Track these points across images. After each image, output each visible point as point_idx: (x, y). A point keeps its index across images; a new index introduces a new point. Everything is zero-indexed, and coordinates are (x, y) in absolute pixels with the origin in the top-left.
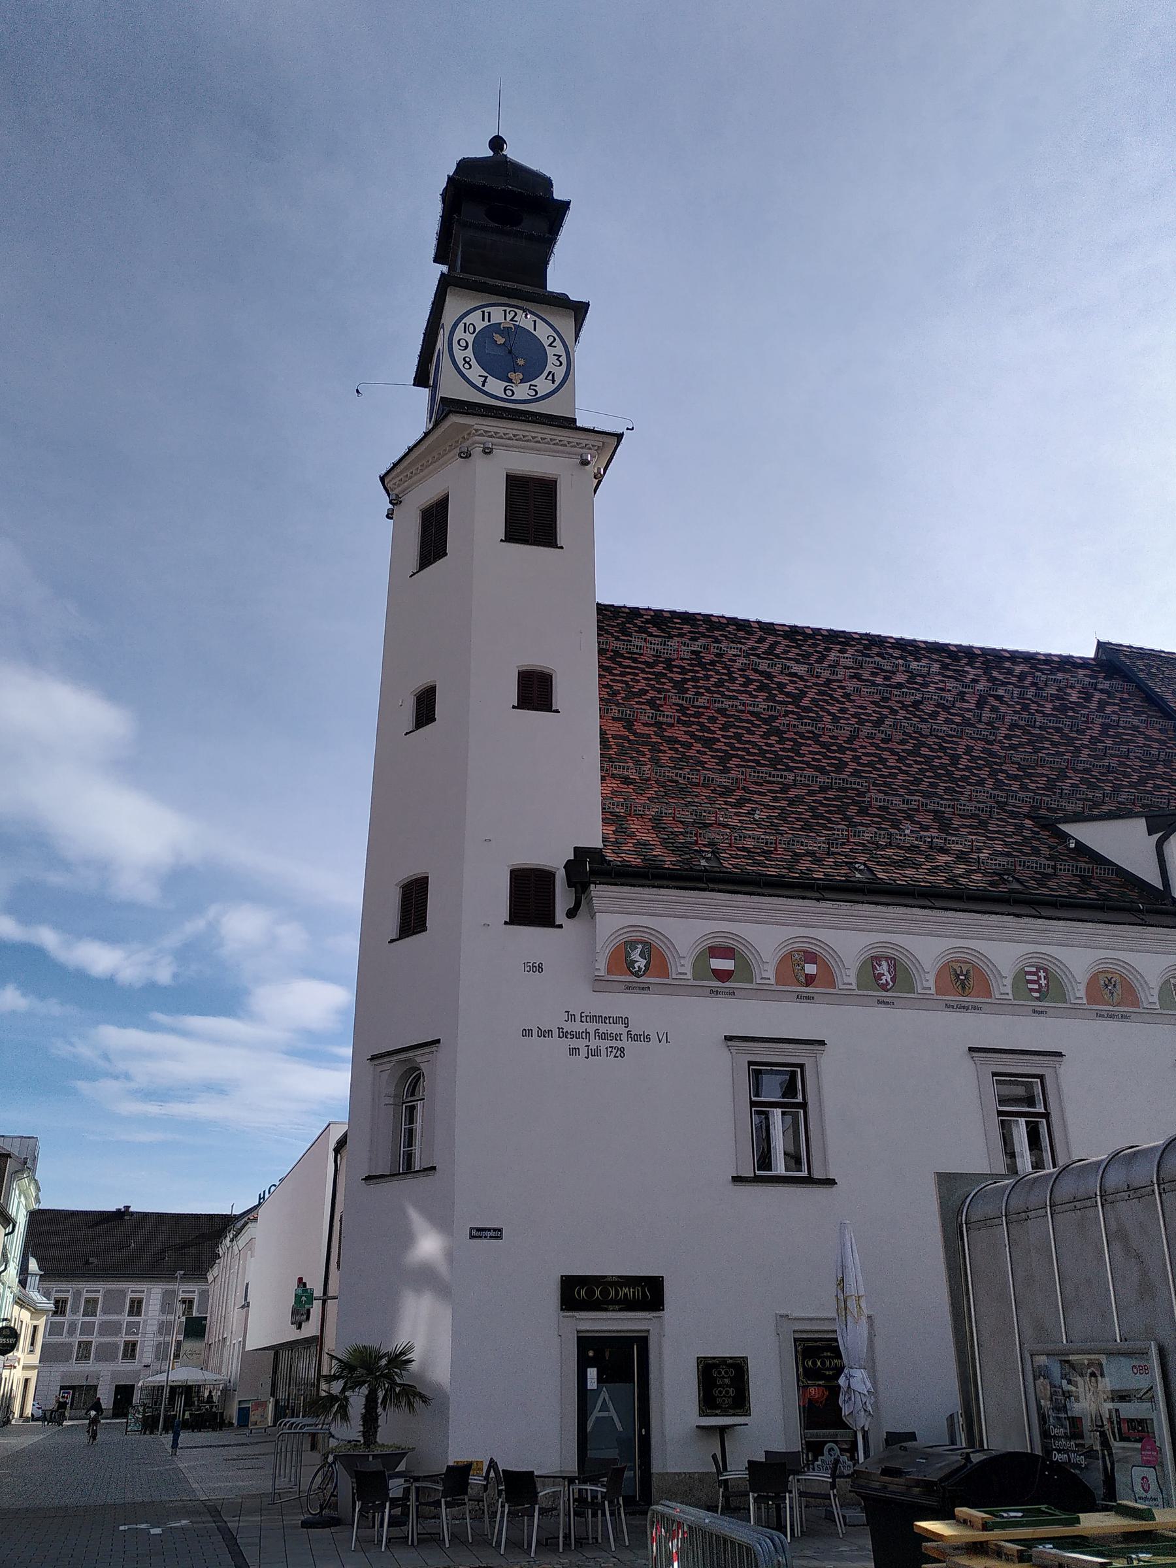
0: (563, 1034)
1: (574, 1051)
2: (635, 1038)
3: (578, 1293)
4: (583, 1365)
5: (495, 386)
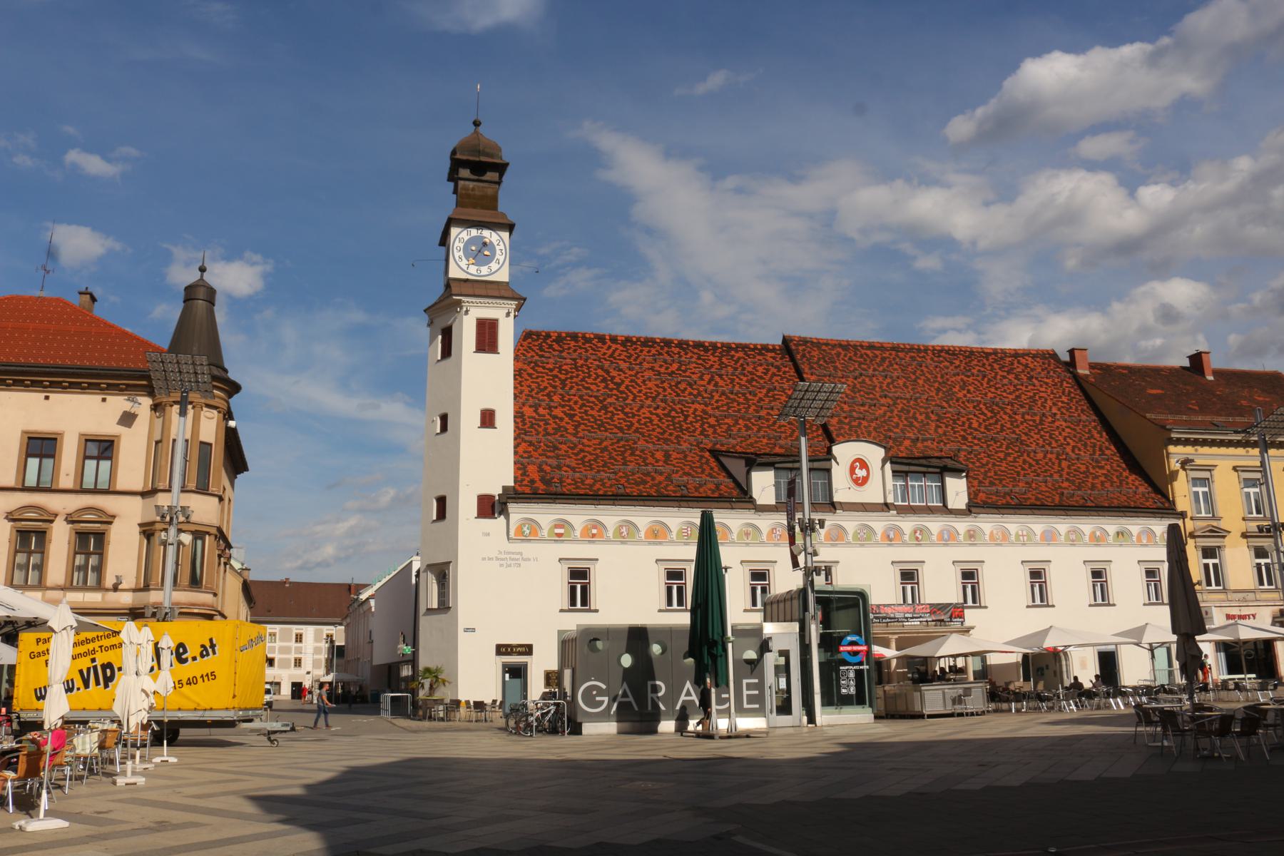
0: (498, 559)
1: (501, 565)
2: (524, 560)
3: (502, 650)
4: (504, 672)
5: (473, 269)
